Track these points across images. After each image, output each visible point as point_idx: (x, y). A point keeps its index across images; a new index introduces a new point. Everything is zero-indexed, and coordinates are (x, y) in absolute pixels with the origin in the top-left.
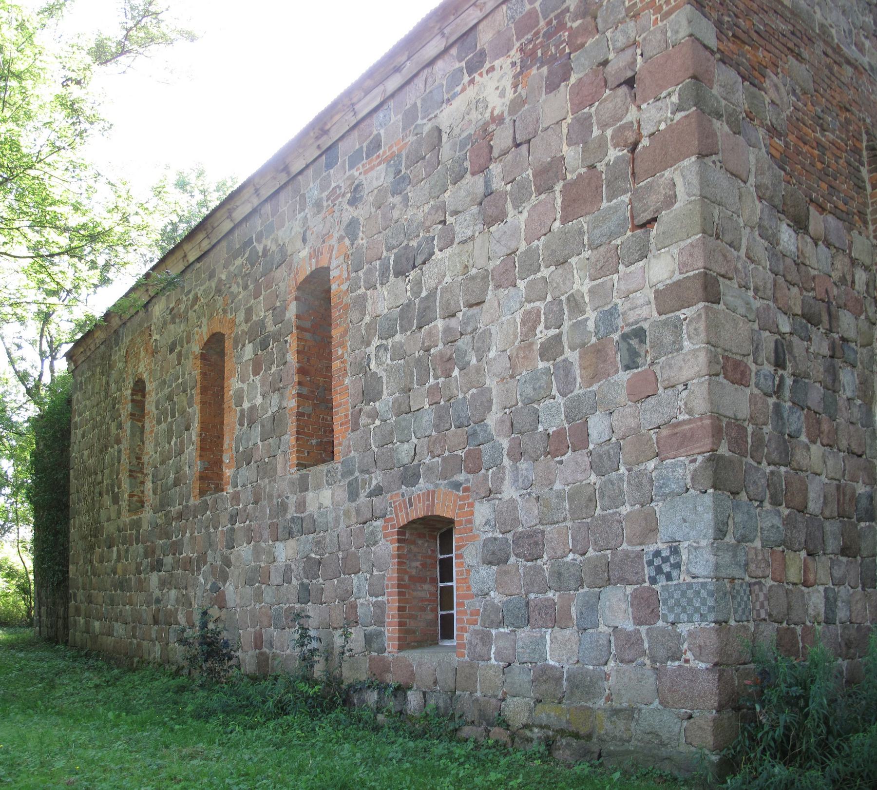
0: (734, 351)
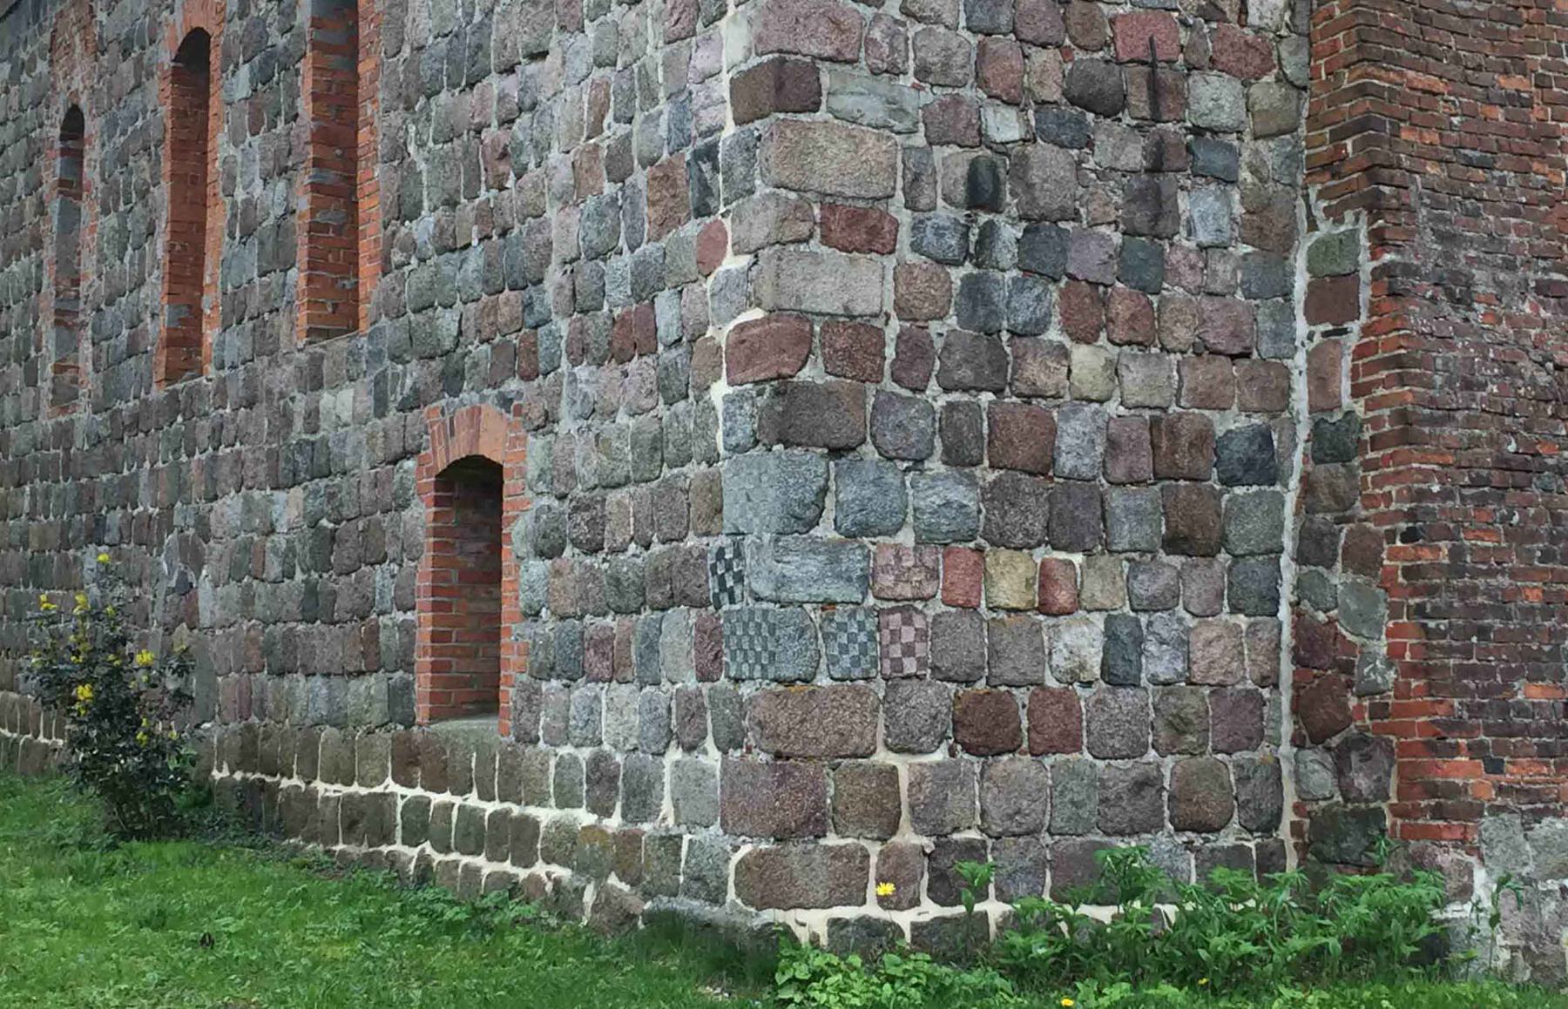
0: (848, 193)
